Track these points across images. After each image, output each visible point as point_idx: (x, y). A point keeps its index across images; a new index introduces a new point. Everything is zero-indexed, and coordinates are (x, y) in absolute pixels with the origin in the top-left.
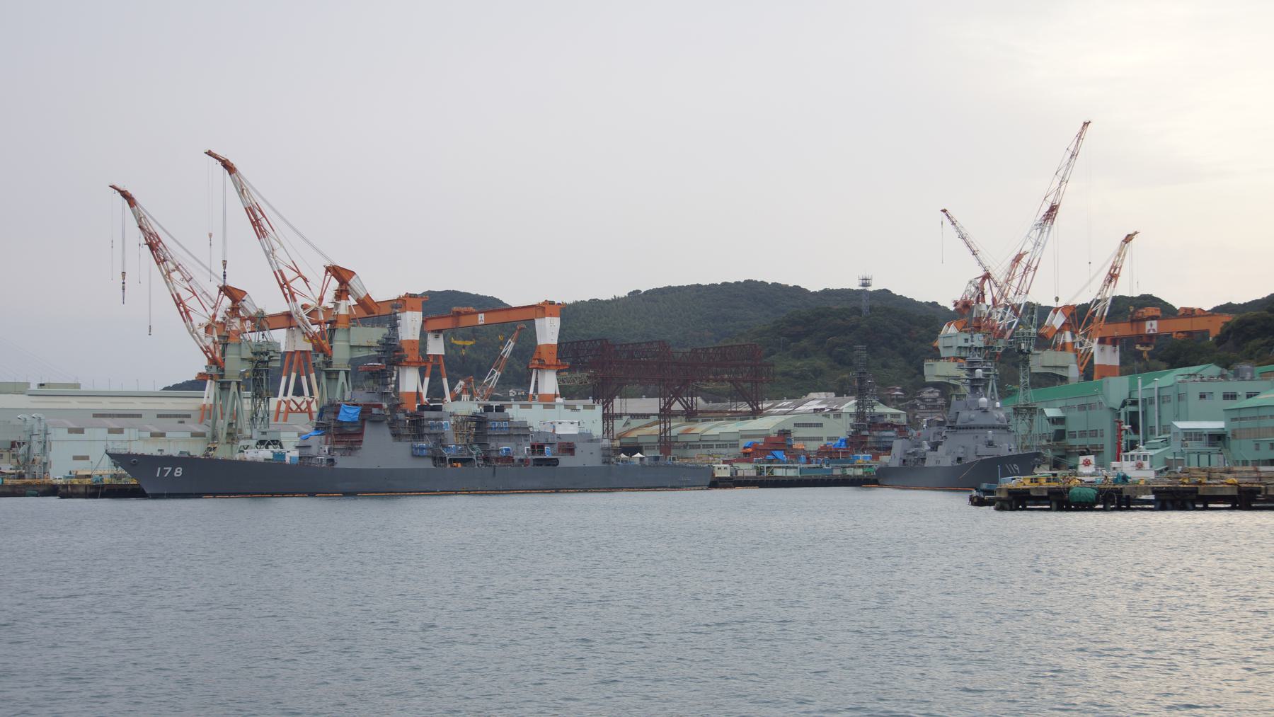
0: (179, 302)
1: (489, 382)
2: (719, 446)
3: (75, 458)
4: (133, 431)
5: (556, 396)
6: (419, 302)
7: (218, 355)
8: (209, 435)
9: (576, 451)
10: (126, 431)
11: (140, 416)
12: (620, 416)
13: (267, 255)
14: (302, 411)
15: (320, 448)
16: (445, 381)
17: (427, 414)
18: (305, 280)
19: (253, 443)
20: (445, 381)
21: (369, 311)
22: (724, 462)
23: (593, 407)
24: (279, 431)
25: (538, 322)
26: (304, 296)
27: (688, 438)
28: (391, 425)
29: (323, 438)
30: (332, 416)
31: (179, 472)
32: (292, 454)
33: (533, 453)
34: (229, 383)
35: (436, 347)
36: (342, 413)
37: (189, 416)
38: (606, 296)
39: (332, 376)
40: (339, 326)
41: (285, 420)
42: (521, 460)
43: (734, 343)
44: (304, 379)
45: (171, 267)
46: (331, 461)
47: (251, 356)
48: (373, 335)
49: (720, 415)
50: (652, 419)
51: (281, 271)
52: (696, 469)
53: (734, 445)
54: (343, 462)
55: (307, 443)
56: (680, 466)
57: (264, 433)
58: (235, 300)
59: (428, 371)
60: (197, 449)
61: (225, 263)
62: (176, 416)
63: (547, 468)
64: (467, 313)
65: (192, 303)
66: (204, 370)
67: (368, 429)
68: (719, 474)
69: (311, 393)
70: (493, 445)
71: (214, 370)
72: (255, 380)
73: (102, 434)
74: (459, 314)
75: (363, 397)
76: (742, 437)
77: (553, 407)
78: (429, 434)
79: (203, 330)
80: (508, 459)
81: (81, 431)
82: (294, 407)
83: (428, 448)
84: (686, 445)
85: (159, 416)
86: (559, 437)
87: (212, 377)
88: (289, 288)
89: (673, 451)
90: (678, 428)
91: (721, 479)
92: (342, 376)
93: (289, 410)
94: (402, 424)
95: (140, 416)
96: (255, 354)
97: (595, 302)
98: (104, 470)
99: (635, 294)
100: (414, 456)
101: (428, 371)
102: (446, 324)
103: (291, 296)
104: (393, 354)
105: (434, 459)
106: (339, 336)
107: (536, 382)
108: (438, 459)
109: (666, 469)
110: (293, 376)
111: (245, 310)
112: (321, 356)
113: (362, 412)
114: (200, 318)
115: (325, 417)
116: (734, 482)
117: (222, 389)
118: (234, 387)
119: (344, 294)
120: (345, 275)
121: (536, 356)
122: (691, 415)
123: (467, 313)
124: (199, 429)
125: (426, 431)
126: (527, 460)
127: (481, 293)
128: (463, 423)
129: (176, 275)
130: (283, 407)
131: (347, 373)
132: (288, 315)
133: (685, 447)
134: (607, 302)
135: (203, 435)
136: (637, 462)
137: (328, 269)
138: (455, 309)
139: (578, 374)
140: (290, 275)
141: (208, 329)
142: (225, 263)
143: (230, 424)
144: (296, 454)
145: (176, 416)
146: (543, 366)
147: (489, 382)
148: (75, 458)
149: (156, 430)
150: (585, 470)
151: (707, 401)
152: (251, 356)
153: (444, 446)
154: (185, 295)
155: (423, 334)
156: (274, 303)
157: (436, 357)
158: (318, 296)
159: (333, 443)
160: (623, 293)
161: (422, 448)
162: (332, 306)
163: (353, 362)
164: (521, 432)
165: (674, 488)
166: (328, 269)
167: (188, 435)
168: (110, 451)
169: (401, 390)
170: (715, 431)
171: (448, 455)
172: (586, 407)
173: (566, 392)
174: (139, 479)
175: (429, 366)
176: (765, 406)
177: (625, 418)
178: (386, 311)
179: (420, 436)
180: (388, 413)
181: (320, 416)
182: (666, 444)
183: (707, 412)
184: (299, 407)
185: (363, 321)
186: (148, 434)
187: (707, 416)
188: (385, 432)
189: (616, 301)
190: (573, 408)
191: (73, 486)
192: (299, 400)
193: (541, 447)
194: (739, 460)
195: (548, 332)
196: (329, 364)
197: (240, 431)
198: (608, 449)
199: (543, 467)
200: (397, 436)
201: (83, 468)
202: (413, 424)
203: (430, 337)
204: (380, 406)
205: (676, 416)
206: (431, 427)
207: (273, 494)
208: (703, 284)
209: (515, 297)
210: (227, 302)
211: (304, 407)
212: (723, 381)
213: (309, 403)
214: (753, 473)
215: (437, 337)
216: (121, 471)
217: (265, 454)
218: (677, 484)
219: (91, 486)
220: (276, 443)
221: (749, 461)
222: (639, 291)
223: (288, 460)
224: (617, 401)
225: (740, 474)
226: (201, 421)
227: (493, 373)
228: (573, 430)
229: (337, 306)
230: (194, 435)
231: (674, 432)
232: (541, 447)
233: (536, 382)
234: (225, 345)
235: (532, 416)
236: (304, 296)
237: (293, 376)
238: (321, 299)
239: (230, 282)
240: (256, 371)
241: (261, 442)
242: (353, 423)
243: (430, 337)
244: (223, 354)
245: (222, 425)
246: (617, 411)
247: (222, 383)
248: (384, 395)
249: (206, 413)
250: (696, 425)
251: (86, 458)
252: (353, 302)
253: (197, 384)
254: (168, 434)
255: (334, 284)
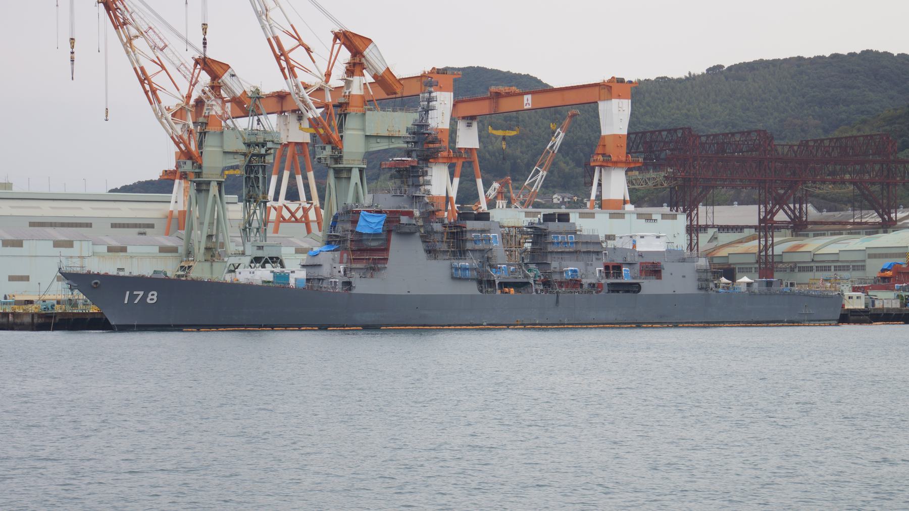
0: (144, 78)
1: (532, 185)
2: (837, 269)
3: (12, 278)
4: (85, 244)
5: (625, 202)
6: (448, 80)
7: (193, 147)
8: (182, 250)
9: (664, 274)
10: (75, 243)
11: (89, 225)
12: (705, 228)
13: (259, 16)
14: (297, 221)
15: (333, 266)
16: (480, 182)
17: (470, 225)
18: (308, 50)
19: (247, 260)
20: (480, 182)
21: (391, 91)
22: (855, 289)
23: (674, 217)
24: (279, 245)
25: (602, 106)
26: (307, 71)
27: (796, 258)
28: (425, 239)
29: (337, 255)
30: (349, 226)
31: (153, 297)
32: (297, 275)
33: (608, 275)
34: (208, 183)
35: (468, 138)
36: (361, 222)
37: (151, 226)
38: (677, 72)
39: (342, 174)
40: (350, 109)
41: (276, 231)
42: (592, 285)
43: (855, 133)
44: (299, 179)
45: (133, 32)
46: (348, 284)
47: (243, 148)
48: (399, 122)
49: (839, 228)
50: (747, 232)
51: (142, 69)
52: (822, 297)
53: (860, 267)
54: (363, 286)
55: (316, 261)
56: (800, 294)
57: (260, 248)
58: (215, 77)
59: (458, 170)
60: (170, 268)
61: (205, 27)
62: (135, 226)
63: (624, 295)
64: (509, 95)
65: (160, 80)
66: (172, 166)
67: (396, 244)
68: (849, 305)
69: (309, 198)
70: (555, 265)
71: (188, 167)
72: (248, 179)
73: (46, 247)
74: (498, 95)
75: (388, 202)
76: (871, 256)
77: (622, 216)
78: (473, 251)
79: (169, 116)
80: (575, 283)
81: (18, 244)
82: (287, 215)
83: (472, 269)
84: (794, 267)
85: (114, 226)
86: (641, 255)
87: (184, 176)
88: (150, 84)
89: (776, 274)
90: (782, 244)
91: (854, 312)
92: (355, 174)
93: (281, 219)
94: (438, 237)
95: (89, 225)
96: (248, 145)
97: (663, 81)
98: (50, 291)
99: (715, 71)
100: (454, 278)
101: (458, 170)
102: (482, 108)
103: (289, 70)
104: (425, 147)
105: (480, 282)
106: (352, 123)
107: (600, 185)
108: (486, 283)
109: (778, 299)
110: (286, 174)
111: (229, 90)
112: (328, 148)
113: (387, 221)
114: (171, 100)
115: (340, 227)
116: (870, 316)
117: (199, 191)
118: (214, 189)
119: (357, 69)
120: (357, 43)
121: (600, 150)
122: (799, 226)
123: (509, 95)
124: (169, 242)
125: (469, 246)
126: (600, 285)
127: (514, 71)
128: (510, 236)
129: (139, 43)
130: (273, 215)
131: (361, 170)
132: (281, 97)
133: (792, 270)
134: (679, 81)
135: (174, 250)
136: (744, 288)
137: (337, 36)
138: (493, 89)
139: (652, 174)
140: (288, 43)
141: (179, 114)
142: (205, 27)
143: (210, 237)
144: (302, 274)
145: (135, 226)
146: (609, 163)
147: (532, 185)
148: (12, 278)
149: (114, 243)
150: (674, 299)
151: (819, 209)
152: (243, 148)
153: (491, 266)
154: (151, 69)
155: (454, 121)
156: (271, 81)
157: (469, 151)
158: (324, 71)
159: (350, 261)
160: (700, 69)
161: (465, 269)
162: (342, 84)
163: (369, 156)
164: (590, 248)
165: (792, 323)
166: (337, 36)
167: (157, 249)
168: (64, 270)
169: (603, 198)
170: (834, 249)
171: (497, 277)
172: (664, 216)
173: (637, 198)
174: (100, 307)
175: (459, 163)
176: (900, 215)
177: (711, 232)
178: (414, 89)
179: (460, 252)
180: (421, 223)
181: (334, 226)
182: (767, 266)
183: (821, 223)
184: (293, 215)
185: (382, 104)
186: (104, 249)
187: (821, 228)
188: (416, 247)
189: (691, 79)
190: (648, 218)
191: (14, 314)
192: (293, 206)
193: (618, 268)
194: (874, 288)
195: (615, 118)
196: (338, 159)
197: (222, 245)
198: (706, 271)
199: (621, 295)
200: (431, 252)
201: (21, 291)
202: (453, 237)
203: (461, 125)
204: (410, 214)
205: (779, 228)
206: (475, 241)
207: (273, 327)
208: (806, 56)
209: (556, 77)
210: (205, 78)
211: (299, 214)
212: (843, 182)
213: (306, 211)
214: (896, 304)
215: (469, 125)
216: (78, 295)
217: (264, 274)
218: (796, 318)
219: (40, 315)
220: (276, 260)
221: (892, 289)
222: (721, 67)
223: (292, 282)
224: (702, 208)
225: (878, 305)
226: (167, 233)
227: (537, 172)
228: (659, 246)
229: (348, 83)
230: (163, 250)
231: (778, 250)
232: (618, 268)
233: (600, 185)
234: (203, 134)
235: (591, 225)
236: (307, 71)
237: (286, 174)
238: (328, 75)
239: (211, 54)
240: (249, 168)
241: (257, 260)
242: (375, 236)
243: (461, 125)
244: (200, 145)
245: (199, 237)
246: (702, 222)
247: (199, 184)
248: (415, 199)
249: (179, 222)
250: (806, 241)
251: (26, 278)
252: (368, 78)
253: (163, 185)
254: (129, 249)
255: (345, 55)
